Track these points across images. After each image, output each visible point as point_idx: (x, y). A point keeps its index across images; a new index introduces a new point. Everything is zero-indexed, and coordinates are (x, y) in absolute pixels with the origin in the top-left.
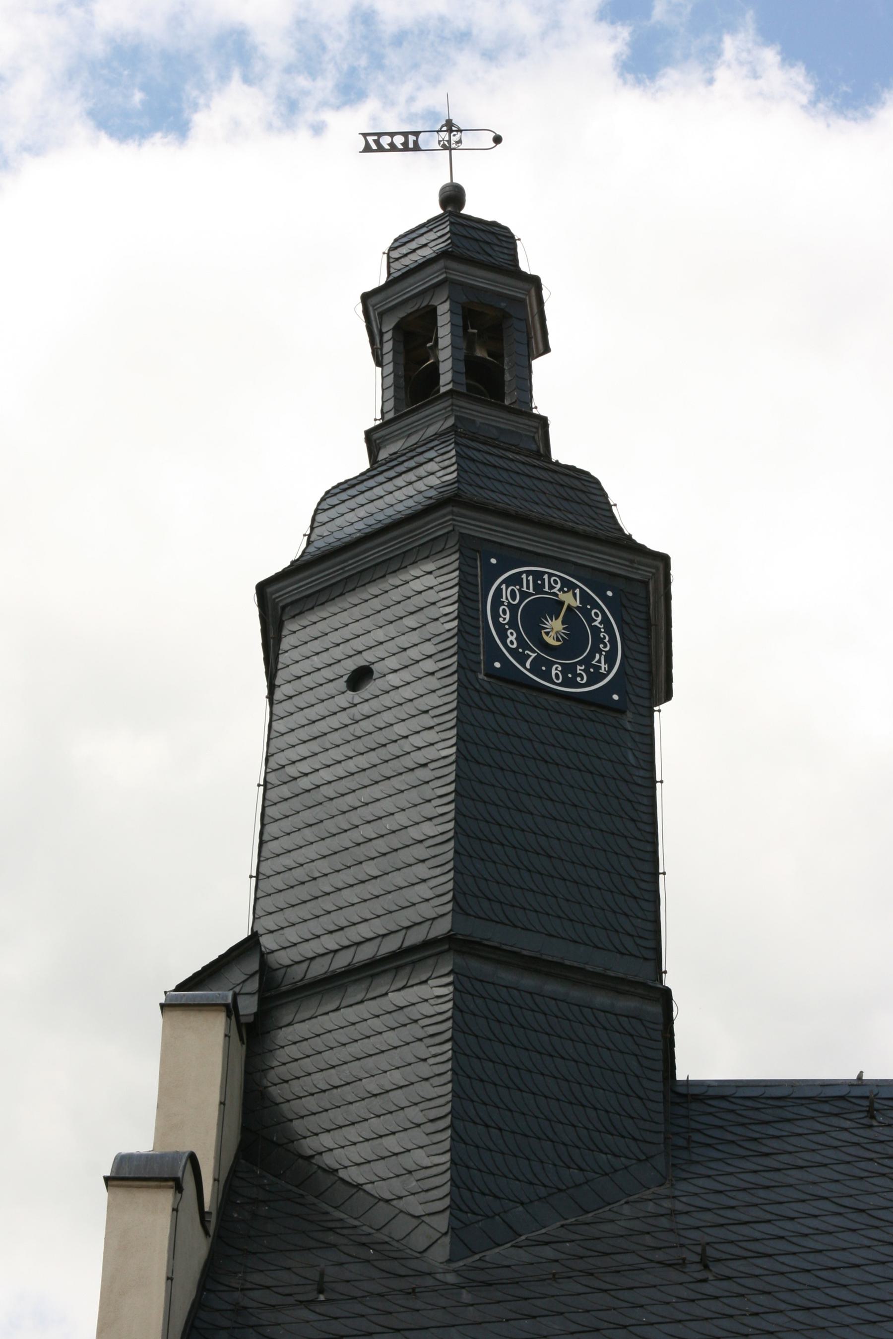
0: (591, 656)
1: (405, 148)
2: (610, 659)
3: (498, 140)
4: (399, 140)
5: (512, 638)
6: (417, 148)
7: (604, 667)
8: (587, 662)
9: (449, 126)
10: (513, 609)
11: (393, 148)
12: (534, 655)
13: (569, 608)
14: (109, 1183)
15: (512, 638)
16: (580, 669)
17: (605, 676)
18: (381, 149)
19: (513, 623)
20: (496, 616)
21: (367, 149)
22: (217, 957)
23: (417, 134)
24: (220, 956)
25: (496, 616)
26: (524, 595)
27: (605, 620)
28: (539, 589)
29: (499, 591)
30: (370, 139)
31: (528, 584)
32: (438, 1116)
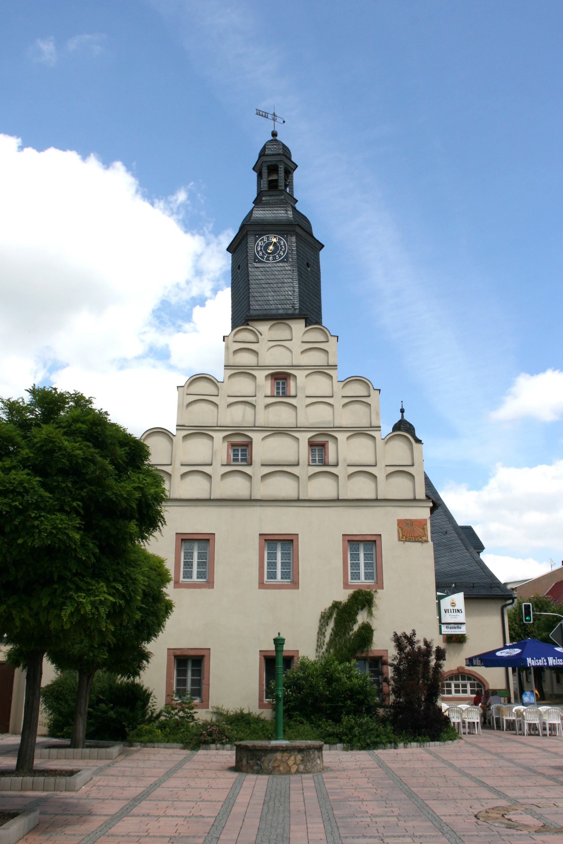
0: (280, 252)
1: (265, 117)
2: (284, 252)
3: (284, 122)
4: (264, 114)
5: (261, 253)
6: (267, 118)
7: (282, 254)
8: (278, 254)
9: (274, 115)
10: (261, 247)
11: (262, 116)
12: (266, 256)
13: (275, 242)
14: (179, 388)
15: (261, 253)
16: (277, 256)
17: (282, 256)
18: (260, 115)
19: (261, 250)
20: (257, 249)
21: (257, 114)
22: (52, 153)
23: (268, 114)
24: (64, 149)
25: (257, 249)
26: (264, 242)
27: (284, 243)
28: (268, 240)
29: (258, 243)
30: (258, 111)
31: (265, 240)
32: (295, 417)
